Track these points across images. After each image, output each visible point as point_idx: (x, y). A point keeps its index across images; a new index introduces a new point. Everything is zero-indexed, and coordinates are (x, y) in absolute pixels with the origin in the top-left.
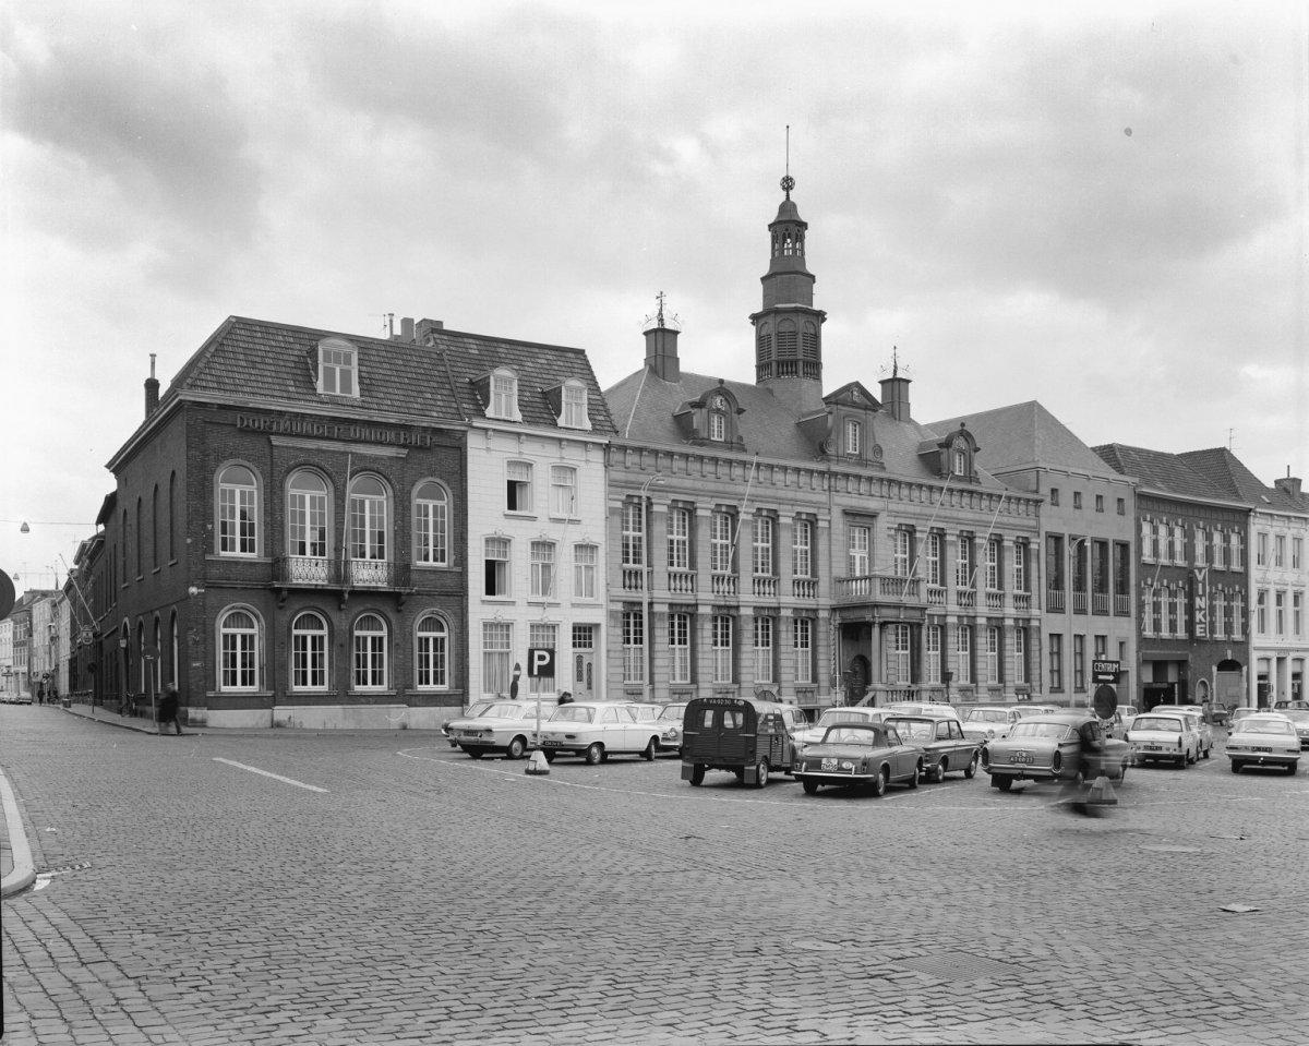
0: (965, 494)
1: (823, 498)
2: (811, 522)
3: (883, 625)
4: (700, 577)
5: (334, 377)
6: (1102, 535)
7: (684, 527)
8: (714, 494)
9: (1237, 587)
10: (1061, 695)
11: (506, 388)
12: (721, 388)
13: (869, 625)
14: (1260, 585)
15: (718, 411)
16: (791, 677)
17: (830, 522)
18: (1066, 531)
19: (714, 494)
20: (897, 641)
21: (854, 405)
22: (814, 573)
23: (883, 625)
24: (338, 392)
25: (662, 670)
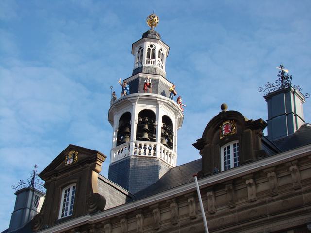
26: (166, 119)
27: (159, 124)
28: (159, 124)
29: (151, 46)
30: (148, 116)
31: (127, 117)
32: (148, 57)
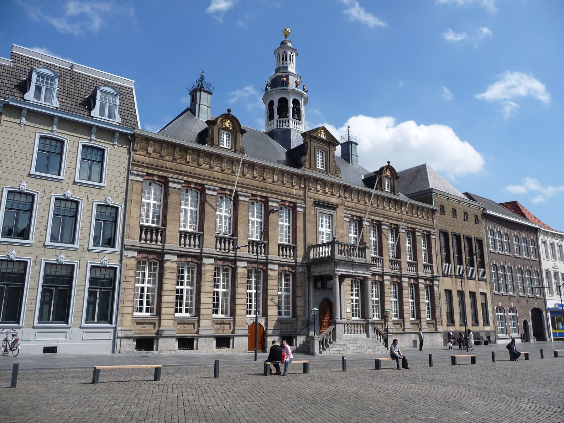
0: (294, 177)
1: (301, 193)
2: (293, 208)
3: (342, 278)
4: (205, 237)
5: (497, 212)
6: (457, 231)
7: (289, 218)
8: (407, 221)
9: (528, 267)
10: (477, 327)
11: (47, 83)
12: (389, 166)
13: (330, 278)
14: (554, 270)
15: (227, 129)
16: (276, 313)
17: (305, 208)
18: (450, 230)
19: (407, 221)
20: (352, 290)
21: (321, 140)
22: (295, 240)
23: (342, 278)
24: (106, 117)
25: (206, 306)
26: (296, 102)
27: (291, 105)
28: (291, 105)
29: (285, 52)
30: (283, 102)
31: (271, 103)
32: (283, 60)
